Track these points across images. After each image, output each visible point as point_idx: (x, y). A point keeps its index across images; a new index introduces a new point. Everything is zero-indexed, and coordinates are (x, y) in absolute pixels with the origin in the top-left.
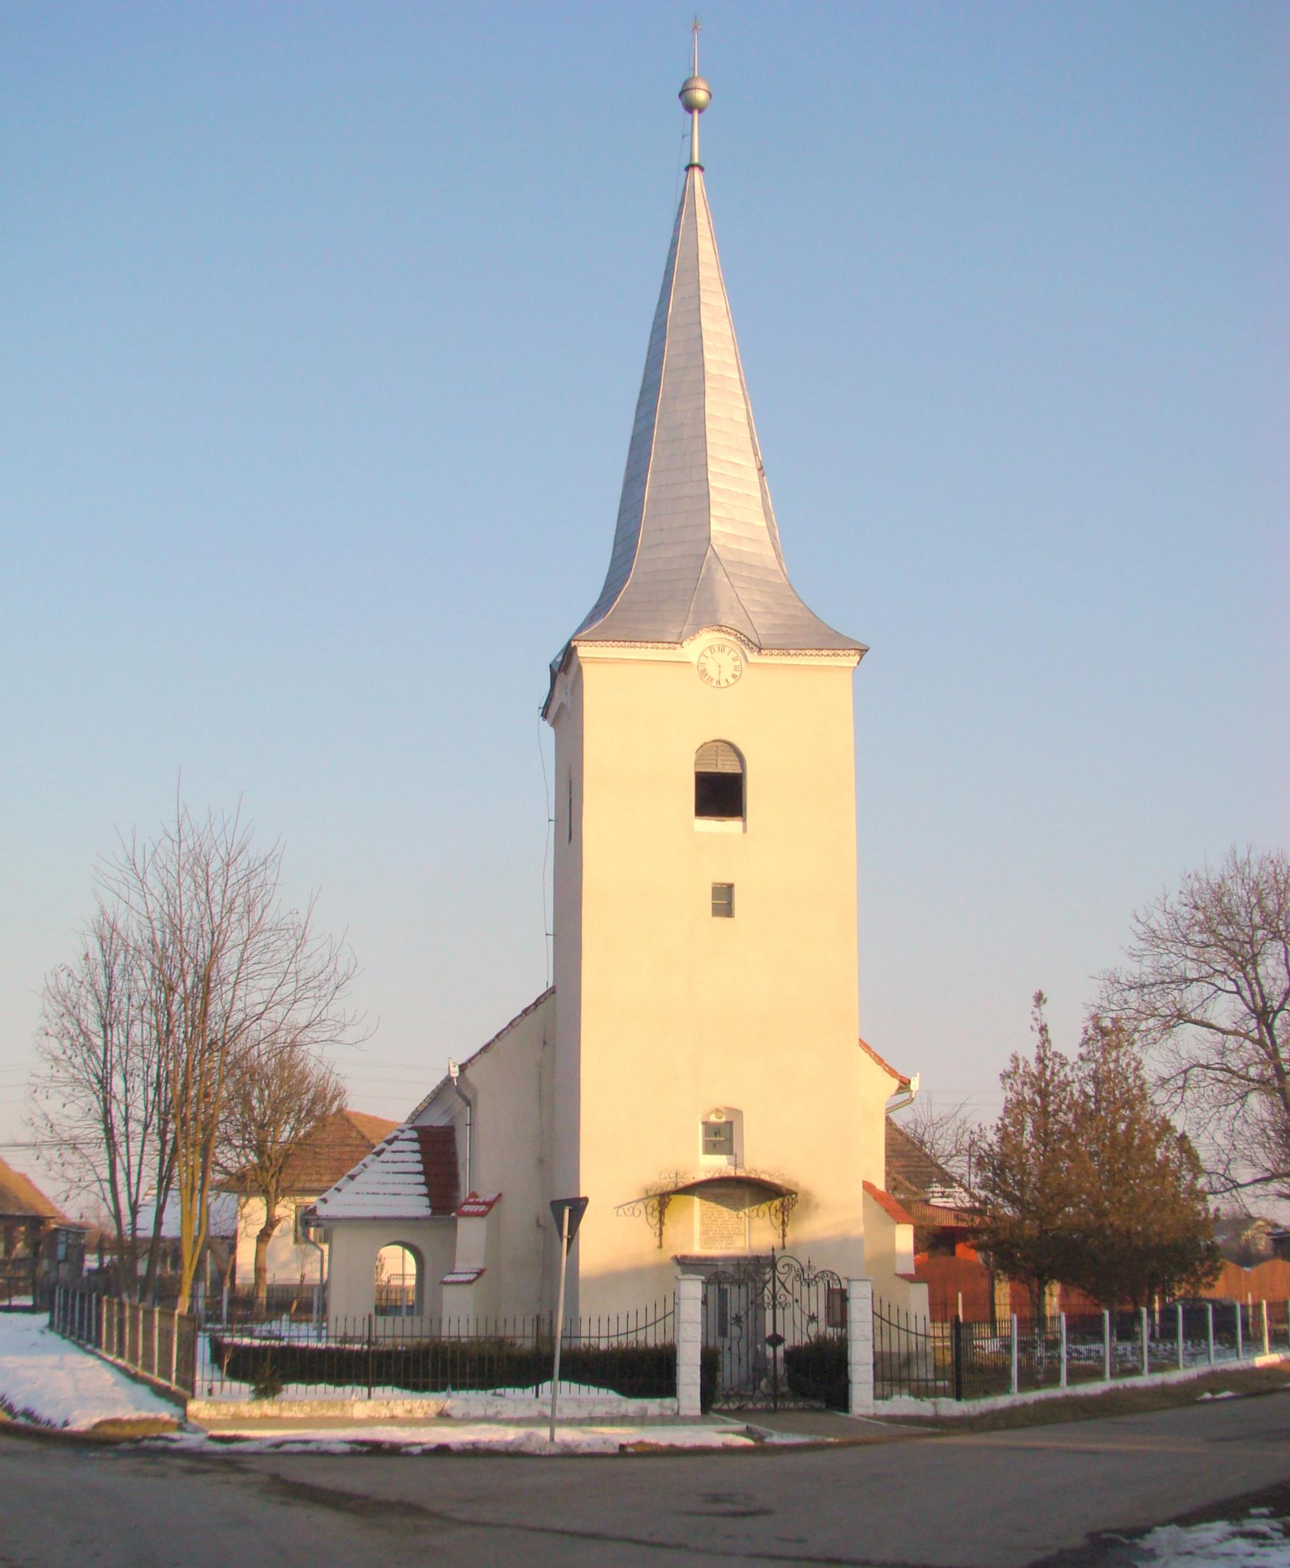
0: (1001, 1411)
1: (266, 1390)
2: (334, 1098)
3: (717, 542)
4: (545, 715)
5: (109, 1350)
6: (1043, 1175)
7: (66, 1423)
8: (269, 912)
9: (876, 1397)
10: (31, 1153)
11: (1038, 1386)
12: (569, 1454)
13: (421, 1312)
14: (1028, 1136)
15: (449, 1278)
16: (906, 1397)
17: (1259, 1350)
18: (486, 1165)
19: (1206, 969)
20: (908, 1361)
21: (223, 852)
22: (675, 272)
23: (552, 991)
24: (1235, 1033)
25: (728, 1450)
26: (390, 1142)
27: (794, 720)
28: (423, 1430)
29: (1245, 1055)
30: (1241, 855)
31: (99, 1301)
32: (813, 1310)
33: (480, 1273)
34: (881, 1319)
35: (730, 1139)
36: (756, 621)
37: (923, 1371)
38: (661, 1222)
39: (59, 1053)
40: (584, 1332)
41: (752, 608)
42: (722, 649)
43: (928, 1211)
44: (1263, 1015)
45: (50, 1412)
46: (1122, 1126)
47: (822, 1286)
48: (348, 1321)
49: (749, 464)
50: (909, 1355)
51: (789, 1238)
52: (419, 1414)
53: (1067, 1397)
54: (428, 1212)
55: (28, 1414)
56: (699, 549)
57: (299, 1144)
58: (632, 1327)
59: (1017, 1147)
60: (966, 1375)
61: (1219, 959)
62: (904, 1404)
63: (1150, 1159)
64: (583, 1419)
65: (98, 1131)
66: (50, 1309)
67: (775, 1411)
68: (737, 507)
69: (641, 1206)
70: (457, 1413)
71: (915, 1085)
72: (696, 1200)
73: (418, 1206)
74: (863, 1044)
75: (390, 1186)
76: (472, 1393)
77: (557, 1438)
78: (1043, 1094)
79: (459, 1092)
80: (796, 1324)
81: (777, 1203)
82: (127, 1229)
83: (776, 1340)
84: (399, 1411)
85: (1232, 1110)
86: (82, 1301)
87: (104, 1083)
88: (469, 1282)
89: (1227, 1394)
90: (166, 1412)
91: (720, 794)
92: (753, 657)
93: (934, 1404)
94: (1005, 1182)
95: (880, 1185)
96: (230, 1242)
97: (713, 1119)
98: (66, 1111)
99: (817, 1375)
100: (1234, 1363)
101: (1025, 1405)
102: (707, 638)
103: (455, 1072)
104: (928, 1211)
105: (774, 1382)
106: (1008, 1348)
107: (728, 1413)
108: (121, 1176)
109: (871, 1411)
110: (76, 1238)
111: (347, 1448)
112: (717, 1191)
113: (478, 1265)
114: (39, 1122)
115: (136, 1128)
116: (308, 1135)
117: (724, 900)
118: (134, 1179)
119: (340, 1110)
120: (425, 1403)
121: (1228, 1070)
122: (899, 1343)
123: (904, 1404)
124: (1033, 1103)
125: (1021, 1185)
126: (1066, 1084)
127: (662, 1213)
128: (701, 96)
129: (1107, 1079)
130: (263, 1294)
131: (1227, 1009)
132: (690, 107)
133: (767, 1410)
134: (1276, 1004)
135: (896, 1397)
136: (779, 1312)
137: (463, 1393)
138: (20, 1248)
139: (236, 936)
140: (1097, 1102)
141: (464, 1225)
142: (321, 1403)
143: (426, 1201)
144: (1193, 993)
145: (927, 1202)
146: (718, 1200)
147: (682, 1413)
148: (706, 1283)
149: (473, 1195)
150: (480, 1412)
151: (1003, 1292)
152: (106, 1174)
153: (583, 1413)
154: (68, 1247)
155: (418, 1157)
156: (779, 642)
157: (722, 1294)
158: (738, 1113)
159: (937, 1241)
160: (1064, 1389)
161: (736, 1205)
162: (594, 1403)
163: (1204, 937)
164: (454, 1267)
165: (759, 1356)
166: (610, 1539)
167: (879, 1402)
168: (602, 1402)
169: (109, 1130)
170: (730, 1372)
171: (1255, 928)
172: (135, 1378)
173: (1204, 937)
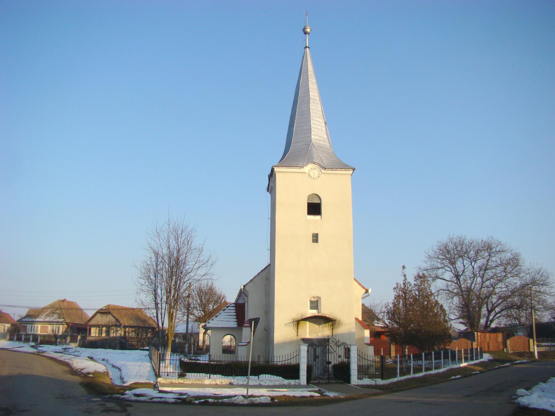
0: (395, 382)
2: (223, 298)
3: (313, 141)
4: (268, 191)
6: (405, 315)
8: (193, 244)
9: (358, 378)
11: (404, 375)
14: (401, 305)
15: (240, 344)
16: (367, 379)
17: (461, 362)
20: (368, 367)
21: (181, 228)
22: (302, 73)
23: (269, 265)
24: (451, 281)
26: (227, 307)
27: (335, 189)
28: (220, 389)
29: (453, 287)
30: (451, 236)
32: (340, 354)
34: (360, 356)
35: (317, 306)
37: (372, 371)
38: (298, 329)
40: (275, 360)
42: (315, 169)
43: (374, 327)
44: (457, 276)
46: (426, 303)
47: (342, 346)
48: (216, 355)
49: (322, 122)
50: (368, 366)
51: (334, 333)
52: (224, 383)
53: (413, 378)
54: (237, 326)
56: (308, 143)
58: (287, 359)
59: (398, 308)
60: (385, 371)
61: (446, 262)
62: (367, 381)
63: (433, 311)
64: (264, 389)
65: (153, 305)
67: (328, 383)
68: (319, 131)
69: (292, 324)
70: (235, 383)
71: (370, 291)
72: (308, 322)
73: (234, 324)
74: (355, 280)
75: (226, 319)
76: (240, 377)
78: (405, 293)
80: (334, 359)
81: (331, 323)
83: (330, 363)
84: (218, 383)
85: (449, 301)
87: (155, 291)
88: (245, 345)
91: (314, 209)
92: (323, 171)
93: (375, 381)
94: (395, 317)
95: (360, 319)
96: (198, 334)
97: (312, 299)
98: (146, 299)
99: (342, 372)
100: (455, 366)
101: (401, 381)
102: (310, 166)
103: (242, 287)
104: (374, 327)
105: (329, 375)
106: (395, 362)
109: (357, 384)
112: (314, 320)
117: (315, 238)
118: (163, 316)
121: (449, 291)
122: (365, 363)
123: (367, 381)
124: (402, 296)
125: (399, 318)
126: (411, 291)
127: (298, 326)
128: (308, 30)
129: (421, 290)
130: (205, 347)
131: (448, 275)
132: (306, 33)
133: (326, 383)
134: (460, 274)
135: (364, 379)
136: (330, 355)
137: (237, 377)
138: (149, 335)
140: (419, 296)
141: (245, 330)
142: (196, 380)
143: (236, 323)
144: (440, 271)
145: (373, 325)
146: (314, 322)
147: (301, 384)
148: (308, 346)
151: (393, 348)
153: (272, 384)
155: (235, 311)
156: (330, 167)
157: (315, 350)
158: (319, 298)
159: (375, 335)
160: (412, 376)
161: (319, 324)
165: (325, 367)
167: (359, 381)
168: (278, 381)
169: (156, 304)
170: (316, 372)
171: (455, 255)
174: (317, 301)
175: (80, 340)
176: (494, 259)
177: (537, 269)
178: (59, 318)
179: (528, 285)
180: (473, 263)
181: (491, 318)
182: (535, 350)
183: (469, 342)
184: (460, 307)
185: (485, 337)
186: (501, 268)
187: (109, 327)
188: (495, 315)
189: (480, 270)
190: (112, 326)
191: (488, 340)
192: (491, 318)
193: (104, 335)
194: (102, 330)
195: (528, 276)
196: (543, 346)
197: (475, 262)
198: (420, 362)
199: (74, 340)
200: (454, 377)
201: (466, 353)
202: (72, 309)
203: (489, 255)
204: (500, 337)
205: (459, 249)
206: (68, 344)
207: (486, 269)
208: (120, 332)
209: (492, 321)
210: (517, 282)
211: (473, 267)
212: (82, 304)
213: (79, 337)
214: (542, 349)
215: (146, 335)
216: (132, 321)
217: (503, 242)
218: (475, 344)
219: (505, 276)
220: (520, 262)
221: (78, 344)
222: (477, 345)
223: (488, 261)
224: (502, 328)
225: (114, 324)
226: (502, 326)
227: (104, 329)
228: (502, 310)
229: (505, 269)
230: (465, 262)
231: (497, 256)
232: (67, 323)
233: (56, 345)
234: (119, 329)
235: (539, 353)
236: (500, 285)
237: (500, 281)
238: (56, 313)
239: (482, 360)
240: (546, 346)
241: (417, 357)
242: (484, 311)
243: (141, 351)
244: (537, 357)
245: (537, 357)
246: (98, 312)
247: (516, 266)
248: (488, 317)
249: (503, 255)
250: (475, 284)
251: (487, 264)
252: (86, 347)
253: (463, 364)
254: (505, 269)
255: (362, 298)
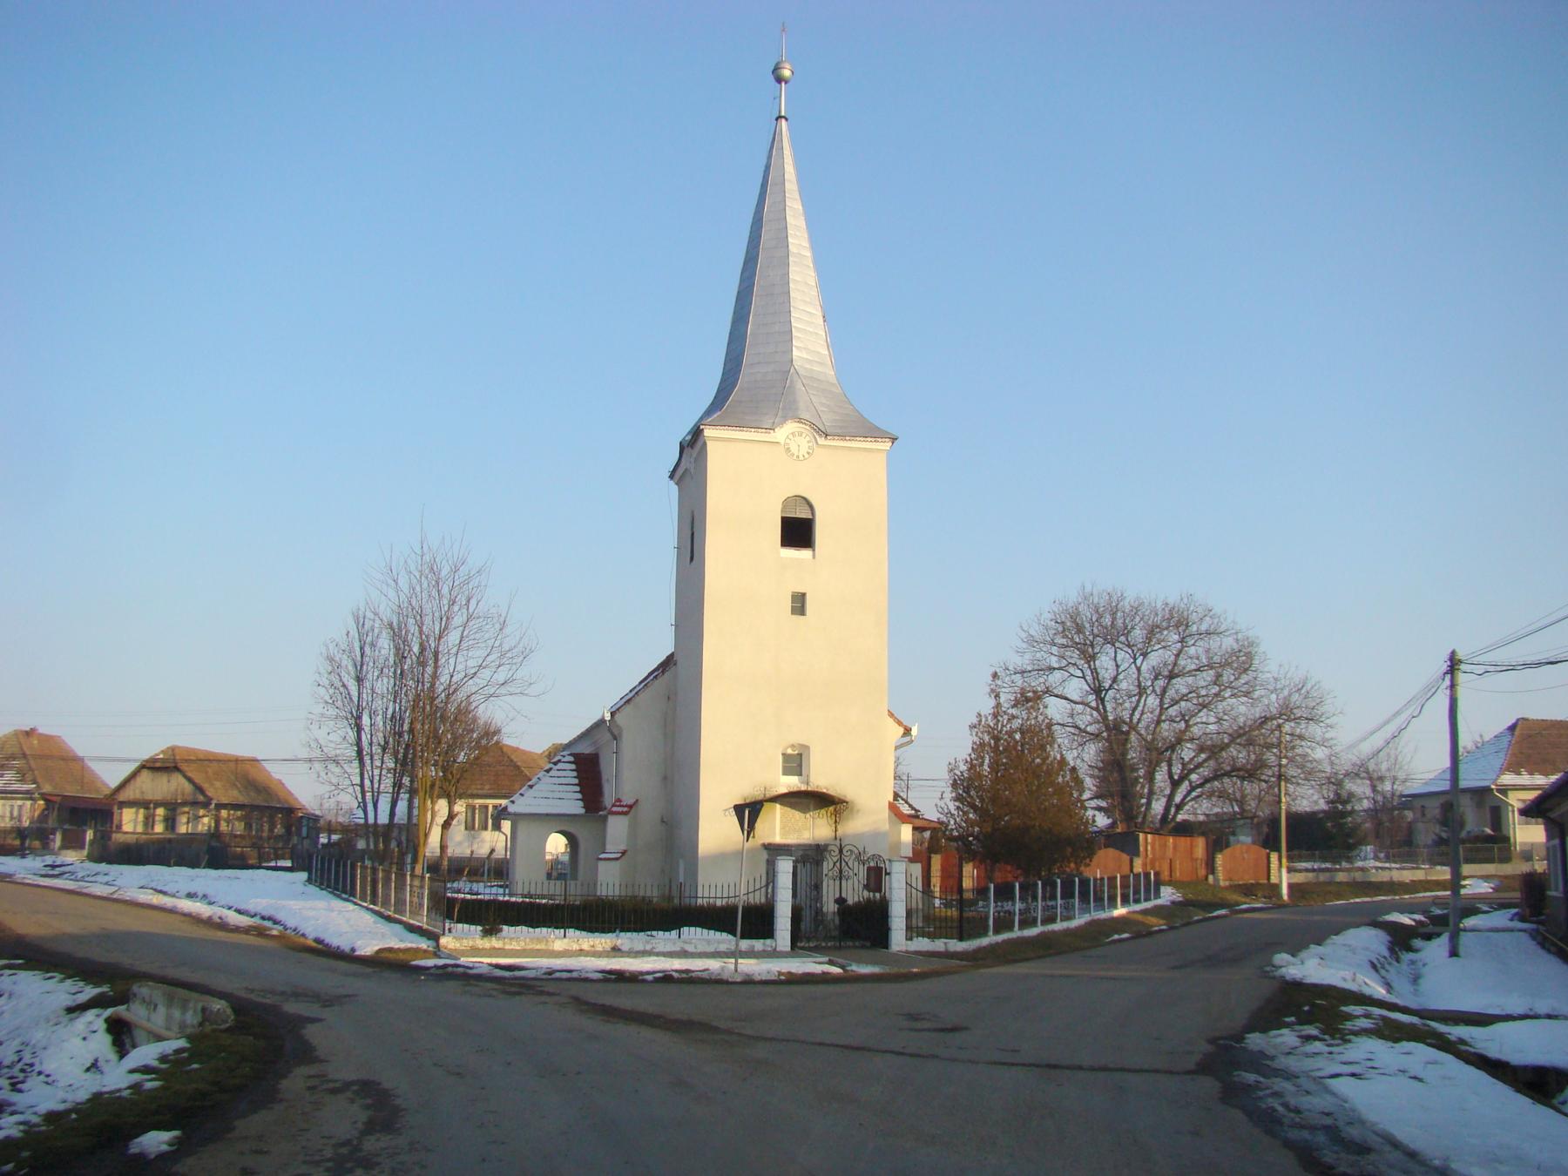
1: (490, 931)
4: (671, 477)
5: (363, 898)
7: (353, 950)
10: (308, 765)
12: (749, 981)
13: (575, 878)
17: (1115, 907)
18: (628, 778)
19: (1064, 663)
23: (668, 664)
25: (824, 979)
27: (849, 485)
29: (1086, 719)
30: (1088, 589)
31: (353, 868)
33: (624, 853)
35: (800, 766)
36: (824, 417)
39: (327, 698)
41: (820, 408)
42: (800, 434)
44: (1098, 691)
45: (335, 941)
48: (527, 883)
55: (318, 941)
57: (471, 764)
66: (308, 869)
67: (840, 948)
68: (810, 341)
70: (625, 948)
71: (914, 732)
73: (577, 807)
75: (556, 793)
77: (740, 968)
79: (609, 729)
82: (371, 821)
84: (586, 946)
86: (337, 866)
89: (1126, 935)
90: (424, 944)
91: (797, 532)
92: (822, 441)
97: (790, 751)
98: (331, 737)
99: (864, 924)
100: (1103, 915)
102: (791, 426)
103: (608, 717)
107: (810, 949)
108: (367, 783)
109: (904, 948)
110: (313, 823)
111: (600, 976)
113: (622, 847)
114: (314, 745)
115: (377, 750)
116: (476, 758)
117: (799, 604)
119: (497, 743)
120: (602, 941)
121: (1076, 727)
128: (787, 73)
131: (1076, 688)
132: (779, 80)
134: (1107, 685)
139: (458, 620)
143: (581, 804)
144: (1058, 675)
146: (792, 806)
149: (619, 800)
150: (640, 947)
152: (357, 780)
153: (711, 949)
154: (309, 828)
158: (807, 748)
160: (1016, 933)
161: (805, 810)
162: (719, 942)
163: (1064, 641)
164: (604, 845)
166: (869, 1050)
168: (723, 942)
169: (360, 752)
171: (1095, 636)
172: (388, 919)
173: (1064, 641)
174: (800, 755)
175: (92, 843)
176: (1192, 651)
177: (1297, 680)
178: (23, 781)
179: (1273, 718)
180: (1139, 662)
181: (1178, 799)
182: (1283, 878)
183: (1125, 857)
184: (1100, 769)
185: (1164, 846)
186: (1209, 675)
187: (172, 808)
188: (1189, 793)
189: (1156, 678)
190: (184, 804)
191: (1170, 853)
192: (1178, 799)
193: (159, 828)
194: (154, 815)
195: (1274, 697)
196: (1300, 871)
197: (1145, 655)
198: (1008, 906)
199: (73, 842)
200: (1116, 937)
201: (1125, 886)
202: (51, 757)
203: (1182, 641)
204: (1200, 845)
205: (1107, 620)
206: (56, 854)
207: (1172, 676)
208: (206, 820)
209: (1179, 807)
210: (1242, 710)
211: (1139, 669)
212: (80, 745)
213: (89, 835)
214: (1299, 878)
215: (271, 830)
216: (235, 793)
217: (1217, 610)
218: (1138, 867)
219: (1216, 695)
220: (1256, 662)
221: (85, 852)
222: (1145, 865)
223: (1177, 656)
224: (1201, 823)
225: (190, 798)
226: (1201, 818)
227: (160, 811)
228: (1207, 781)
229: (1219, 676)
230: (1121, 655)
231: (1200, 643)
232: (44, 797)
233: (23, 856)
234: (202, 812)
235: (1290, 886)
236: (1203, 716)
237: (1204, 706)
238: (11, 768)
239: (1159, 902)
240: (1307, 870)
241: (1004, 893)
242: (1161, 776)
243: (270, 872)
244: (1285, 898)
245: (1285, 898)
246: (143, 767)
247: (1246, 670)
248: (1170, 797)
249: (1214, 643)
250: (1142, 713)
251: (1175, 664)
252: (110, 862)
253: (1120, 911)
254: (1219, 676)
255: (897, 748)
